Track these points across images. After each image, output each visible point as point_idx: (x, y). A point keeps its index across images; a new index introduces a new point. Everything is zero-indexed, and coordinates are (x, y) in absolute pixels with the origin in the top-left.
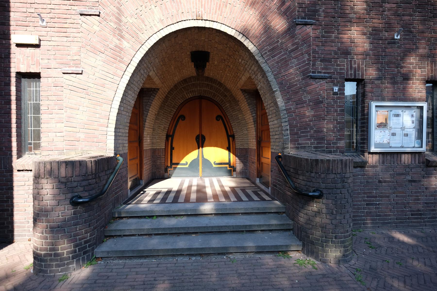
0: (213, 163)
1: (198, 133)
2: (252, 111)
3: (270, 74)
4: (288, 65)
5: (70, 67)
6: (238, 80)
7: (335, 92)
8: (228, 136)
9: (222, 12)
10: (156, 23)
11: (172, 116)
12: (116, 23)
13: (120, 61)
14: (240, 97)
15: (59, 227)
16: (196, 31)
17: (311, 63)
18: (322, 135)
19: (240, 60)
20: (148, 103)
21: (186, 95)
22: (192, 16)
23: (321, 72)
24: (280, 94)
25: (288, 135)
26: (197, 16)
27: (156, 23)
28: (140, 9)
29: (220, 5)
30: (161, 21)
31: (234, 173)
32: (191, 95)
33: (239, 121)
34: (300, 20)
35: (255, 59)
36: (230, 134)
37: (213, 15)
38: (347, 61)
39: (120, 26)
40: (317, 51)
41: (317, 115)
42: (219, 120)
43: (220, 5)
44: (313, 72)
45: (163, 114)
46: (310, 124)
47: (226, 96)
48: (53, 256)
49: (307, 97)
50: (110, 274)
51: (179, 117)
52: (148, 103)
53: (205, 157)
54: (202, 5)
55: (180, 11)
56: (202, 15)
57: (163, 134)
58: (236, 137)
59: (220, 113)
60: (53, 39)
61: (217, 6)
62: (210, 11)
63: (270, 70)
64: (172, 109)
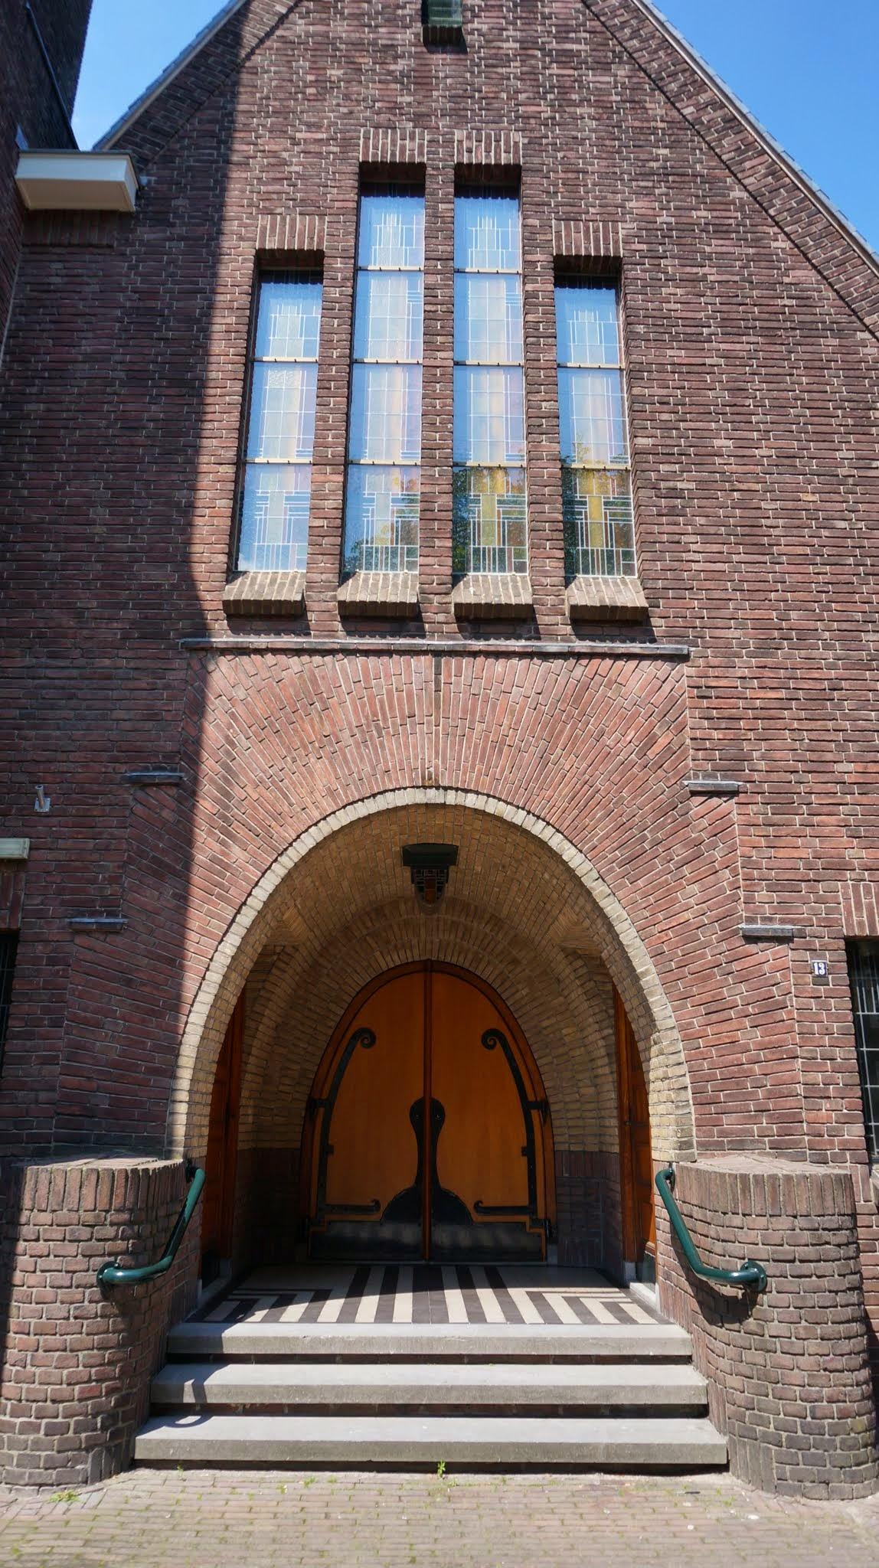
0: (470, 1206)
1: (418, 1094)
2: (598, 1017)
3: (626, 925)
4: (675, 901)
5: (92, 914)
6: (550, 920)
7: (820, 976)
8: (527, 1106)
9: (488, 768)
10: (319, 798)
11: (330, 1032)
12: (217, 801)
13: (219, 897)
14: (563, 968)
15: (65, 1350)
16: (423, 810)
17: (741, 893)
18: (793, 1105)
19: (546, 876)
20: (262, 993)
21: (380, 959)
22: (412, 780)
23: (770, 920)
24: (657, 982)
25: (688, 1105)
26: (423, 778)
27: (319, 798)
28: (281, 764)
29: (484, 750)
30: (332, 793)
31: (552, 1248)
32: (396, 957)
33: (566, 1049)
34: (701, 781)
35: (582, 885)
36: (531, 1097)
37: (465, 774)
38: (846, 887)
39: (227, 808)
40: (756, 862)
41: (770, 1042)
42: (492, 1047)
43: (484, 750)
44: (751, 920)
45: (302, 1024)
46: (751, 1070)
47: (515, 962)
48: (42, 1432)
49: (738, 994)
50: (181, 1496)
51: (354, 1037)
52: (262, 993)
53: (445, 1184)
54: (437, 753)
55: (381, 766)
56: (437, 775)
57: (297, 1096)
58: (553, 1108)
59: (494, 1022)
60: (61, 843)
61: (475, 753)
62: (459, 764)
63: (625, 914)
64: (333, 1007)
